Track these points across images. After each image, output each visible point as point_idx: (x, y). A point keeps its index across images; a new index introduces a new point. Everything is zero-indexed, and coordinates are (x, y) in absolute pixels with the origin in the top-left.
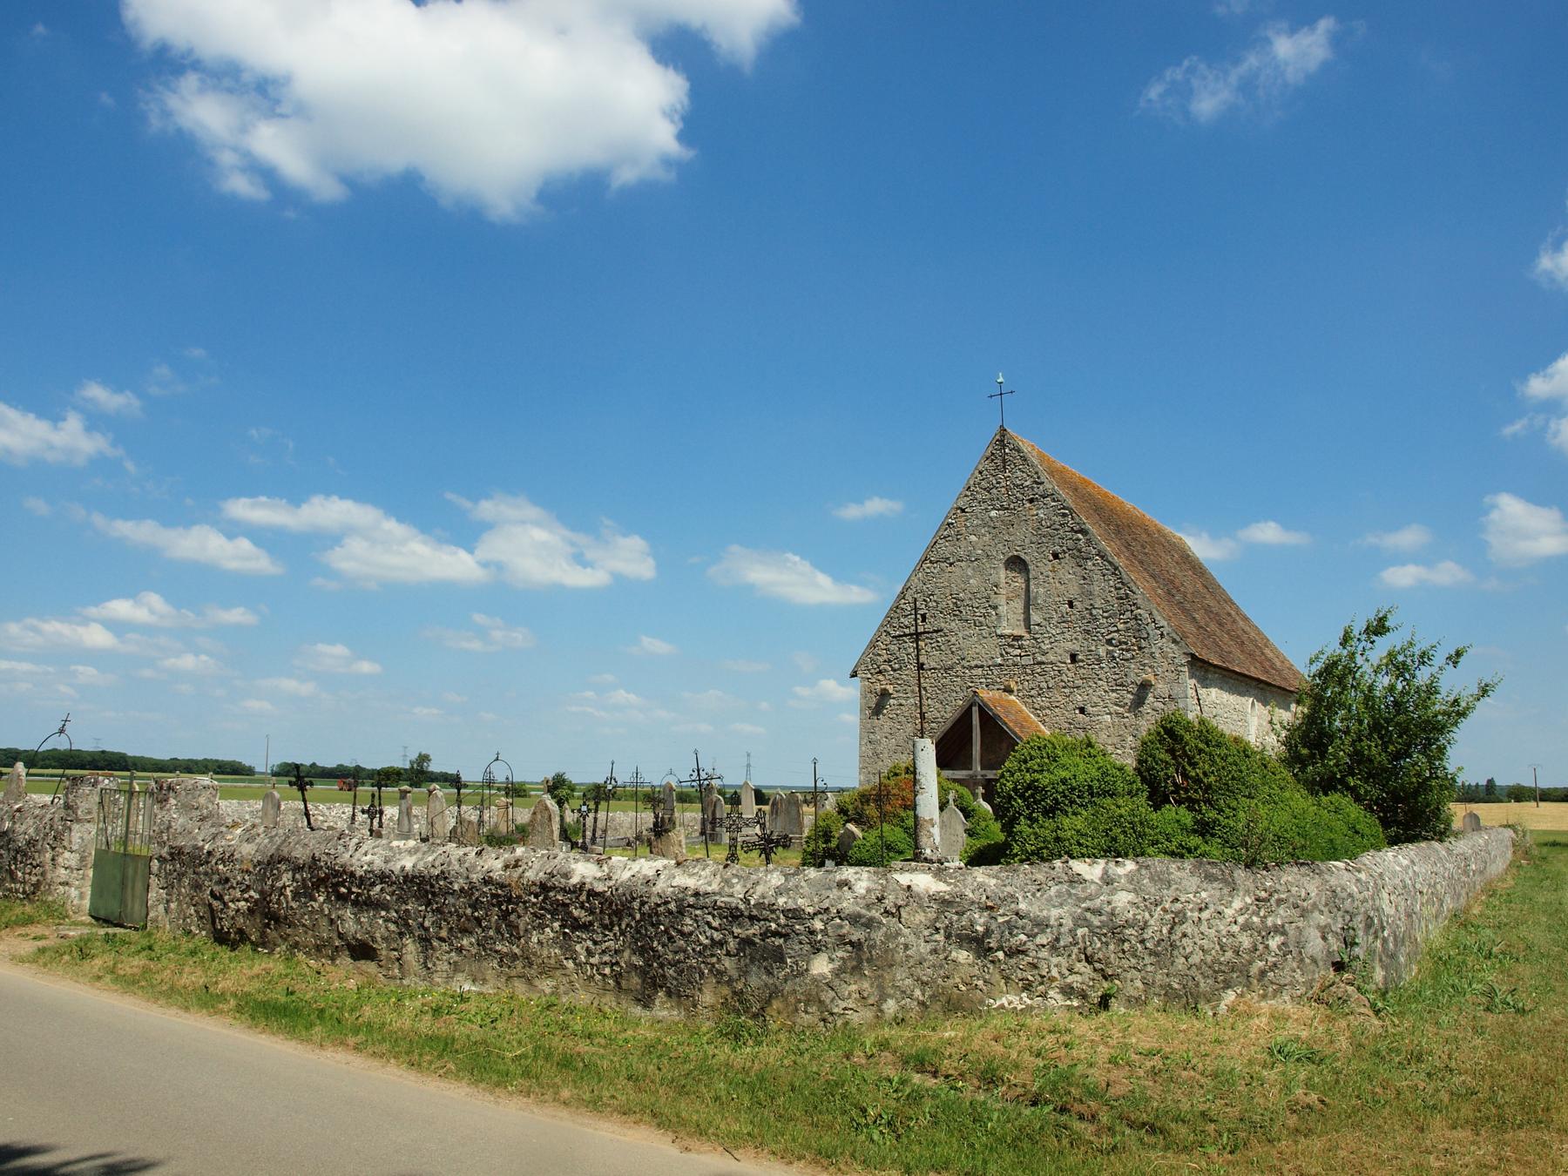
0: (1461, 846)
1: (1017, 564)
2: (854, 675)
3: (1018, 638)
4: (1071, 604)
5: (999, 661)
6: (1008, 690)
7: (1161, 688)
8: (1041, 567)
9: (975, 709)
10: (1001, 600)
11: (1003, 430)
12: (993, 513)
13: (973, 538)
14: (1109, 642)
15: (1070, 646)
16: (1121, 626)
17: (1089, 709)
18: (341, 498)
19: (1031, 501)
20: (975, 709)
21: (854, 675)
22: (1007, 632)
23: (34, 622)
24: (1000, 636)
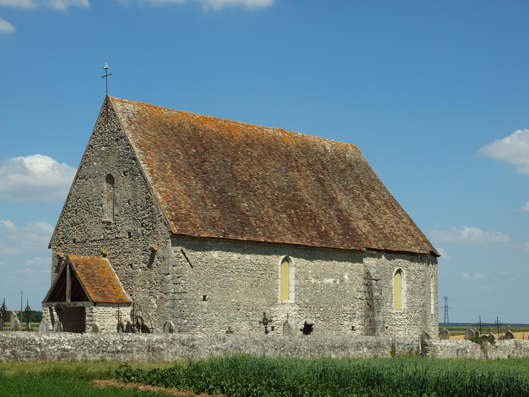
0: (174, 334)
1: (110, 179)
2: (50, 247)
3: (109, 223)
4: (129, 202)
5: (102, 237)
6: (105, 256)
7: (160, 252)
8: (119, 180)
9: (68, 266)
10: (104, 201)
11: (107, 97)
12: (103, 148)
13: (95, 163)
14: (142, 226)
15: (127, 227)
16: (147, 215)
17: (134, 265)
18: (42, 155)
19: (117, 140)
20: (68, 266)
21: (50, 247)
22: (106, 220)
23: (185, 250)
24: (103, 222)
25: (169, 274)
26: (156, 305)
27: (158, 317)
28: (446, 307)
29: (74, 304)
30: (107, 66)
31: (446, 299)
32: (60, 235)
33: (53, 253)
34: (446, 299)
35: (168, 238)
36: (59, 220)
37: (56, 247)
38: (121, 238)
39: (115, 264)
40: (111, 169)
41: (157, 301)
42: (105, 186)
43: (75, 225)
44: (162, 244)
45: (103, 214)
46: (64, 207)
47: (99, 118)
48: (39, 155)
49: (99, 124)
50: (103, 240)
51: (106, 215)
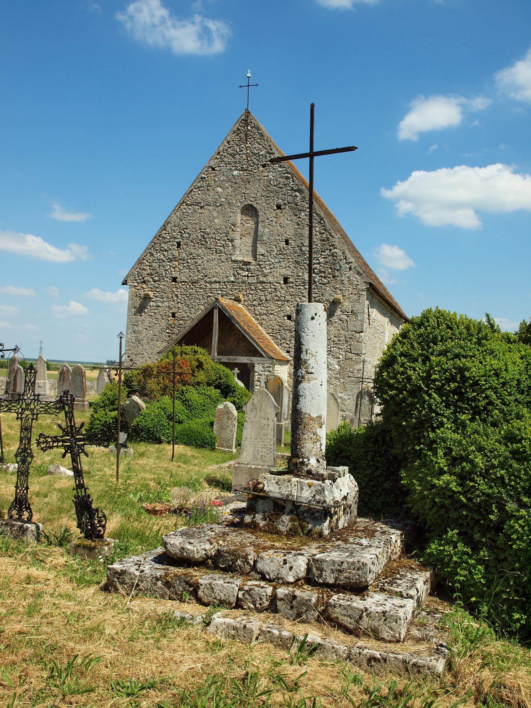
1: (250, 210)
5: (232, 279)
6: (239, 301)
7: (347, 305)
11: (248, 112)
20: (216, 312)
21: (125, 283)
22: (239, 258)
24: (234, 261)
25: (362, 332)
26: (337, 366)
27: (342, 381)
28: (41, 348)
29: (227, 359)
30: (249, 75)
31: (41, 342)
32: (145, 270)
33: (132, 291)
34: (41, 342)
35: (362, 290)
36: (145, 252)
37: (136, 284)
38: (270, 283)
39: (257, 313)
40: (252, 199)
41: (339, 362)
42: (239, 218)
43: (178, 261)
44: (351, 296)
45: (235, 251)
46: (155, 237)
47: (228, 135)
48: (464, 167)
49: (228, 142)
50: (233, 282)
51: (238, 253)
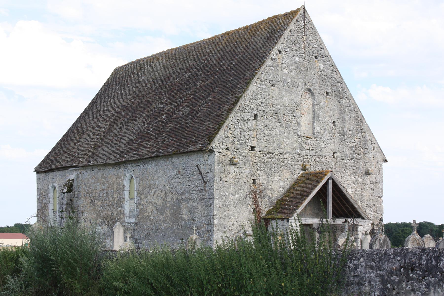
9: (330, 181)
20: (330, 181)
